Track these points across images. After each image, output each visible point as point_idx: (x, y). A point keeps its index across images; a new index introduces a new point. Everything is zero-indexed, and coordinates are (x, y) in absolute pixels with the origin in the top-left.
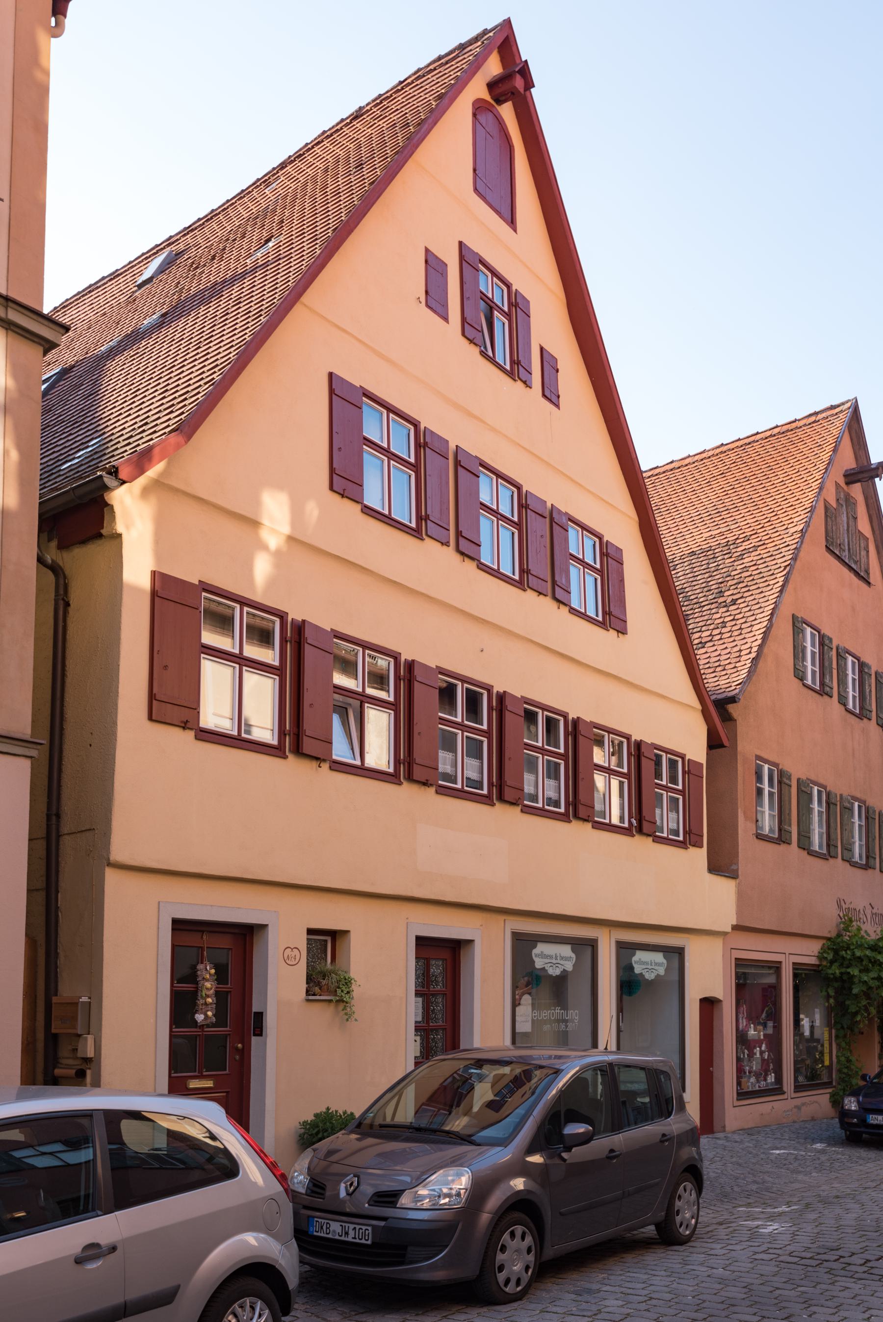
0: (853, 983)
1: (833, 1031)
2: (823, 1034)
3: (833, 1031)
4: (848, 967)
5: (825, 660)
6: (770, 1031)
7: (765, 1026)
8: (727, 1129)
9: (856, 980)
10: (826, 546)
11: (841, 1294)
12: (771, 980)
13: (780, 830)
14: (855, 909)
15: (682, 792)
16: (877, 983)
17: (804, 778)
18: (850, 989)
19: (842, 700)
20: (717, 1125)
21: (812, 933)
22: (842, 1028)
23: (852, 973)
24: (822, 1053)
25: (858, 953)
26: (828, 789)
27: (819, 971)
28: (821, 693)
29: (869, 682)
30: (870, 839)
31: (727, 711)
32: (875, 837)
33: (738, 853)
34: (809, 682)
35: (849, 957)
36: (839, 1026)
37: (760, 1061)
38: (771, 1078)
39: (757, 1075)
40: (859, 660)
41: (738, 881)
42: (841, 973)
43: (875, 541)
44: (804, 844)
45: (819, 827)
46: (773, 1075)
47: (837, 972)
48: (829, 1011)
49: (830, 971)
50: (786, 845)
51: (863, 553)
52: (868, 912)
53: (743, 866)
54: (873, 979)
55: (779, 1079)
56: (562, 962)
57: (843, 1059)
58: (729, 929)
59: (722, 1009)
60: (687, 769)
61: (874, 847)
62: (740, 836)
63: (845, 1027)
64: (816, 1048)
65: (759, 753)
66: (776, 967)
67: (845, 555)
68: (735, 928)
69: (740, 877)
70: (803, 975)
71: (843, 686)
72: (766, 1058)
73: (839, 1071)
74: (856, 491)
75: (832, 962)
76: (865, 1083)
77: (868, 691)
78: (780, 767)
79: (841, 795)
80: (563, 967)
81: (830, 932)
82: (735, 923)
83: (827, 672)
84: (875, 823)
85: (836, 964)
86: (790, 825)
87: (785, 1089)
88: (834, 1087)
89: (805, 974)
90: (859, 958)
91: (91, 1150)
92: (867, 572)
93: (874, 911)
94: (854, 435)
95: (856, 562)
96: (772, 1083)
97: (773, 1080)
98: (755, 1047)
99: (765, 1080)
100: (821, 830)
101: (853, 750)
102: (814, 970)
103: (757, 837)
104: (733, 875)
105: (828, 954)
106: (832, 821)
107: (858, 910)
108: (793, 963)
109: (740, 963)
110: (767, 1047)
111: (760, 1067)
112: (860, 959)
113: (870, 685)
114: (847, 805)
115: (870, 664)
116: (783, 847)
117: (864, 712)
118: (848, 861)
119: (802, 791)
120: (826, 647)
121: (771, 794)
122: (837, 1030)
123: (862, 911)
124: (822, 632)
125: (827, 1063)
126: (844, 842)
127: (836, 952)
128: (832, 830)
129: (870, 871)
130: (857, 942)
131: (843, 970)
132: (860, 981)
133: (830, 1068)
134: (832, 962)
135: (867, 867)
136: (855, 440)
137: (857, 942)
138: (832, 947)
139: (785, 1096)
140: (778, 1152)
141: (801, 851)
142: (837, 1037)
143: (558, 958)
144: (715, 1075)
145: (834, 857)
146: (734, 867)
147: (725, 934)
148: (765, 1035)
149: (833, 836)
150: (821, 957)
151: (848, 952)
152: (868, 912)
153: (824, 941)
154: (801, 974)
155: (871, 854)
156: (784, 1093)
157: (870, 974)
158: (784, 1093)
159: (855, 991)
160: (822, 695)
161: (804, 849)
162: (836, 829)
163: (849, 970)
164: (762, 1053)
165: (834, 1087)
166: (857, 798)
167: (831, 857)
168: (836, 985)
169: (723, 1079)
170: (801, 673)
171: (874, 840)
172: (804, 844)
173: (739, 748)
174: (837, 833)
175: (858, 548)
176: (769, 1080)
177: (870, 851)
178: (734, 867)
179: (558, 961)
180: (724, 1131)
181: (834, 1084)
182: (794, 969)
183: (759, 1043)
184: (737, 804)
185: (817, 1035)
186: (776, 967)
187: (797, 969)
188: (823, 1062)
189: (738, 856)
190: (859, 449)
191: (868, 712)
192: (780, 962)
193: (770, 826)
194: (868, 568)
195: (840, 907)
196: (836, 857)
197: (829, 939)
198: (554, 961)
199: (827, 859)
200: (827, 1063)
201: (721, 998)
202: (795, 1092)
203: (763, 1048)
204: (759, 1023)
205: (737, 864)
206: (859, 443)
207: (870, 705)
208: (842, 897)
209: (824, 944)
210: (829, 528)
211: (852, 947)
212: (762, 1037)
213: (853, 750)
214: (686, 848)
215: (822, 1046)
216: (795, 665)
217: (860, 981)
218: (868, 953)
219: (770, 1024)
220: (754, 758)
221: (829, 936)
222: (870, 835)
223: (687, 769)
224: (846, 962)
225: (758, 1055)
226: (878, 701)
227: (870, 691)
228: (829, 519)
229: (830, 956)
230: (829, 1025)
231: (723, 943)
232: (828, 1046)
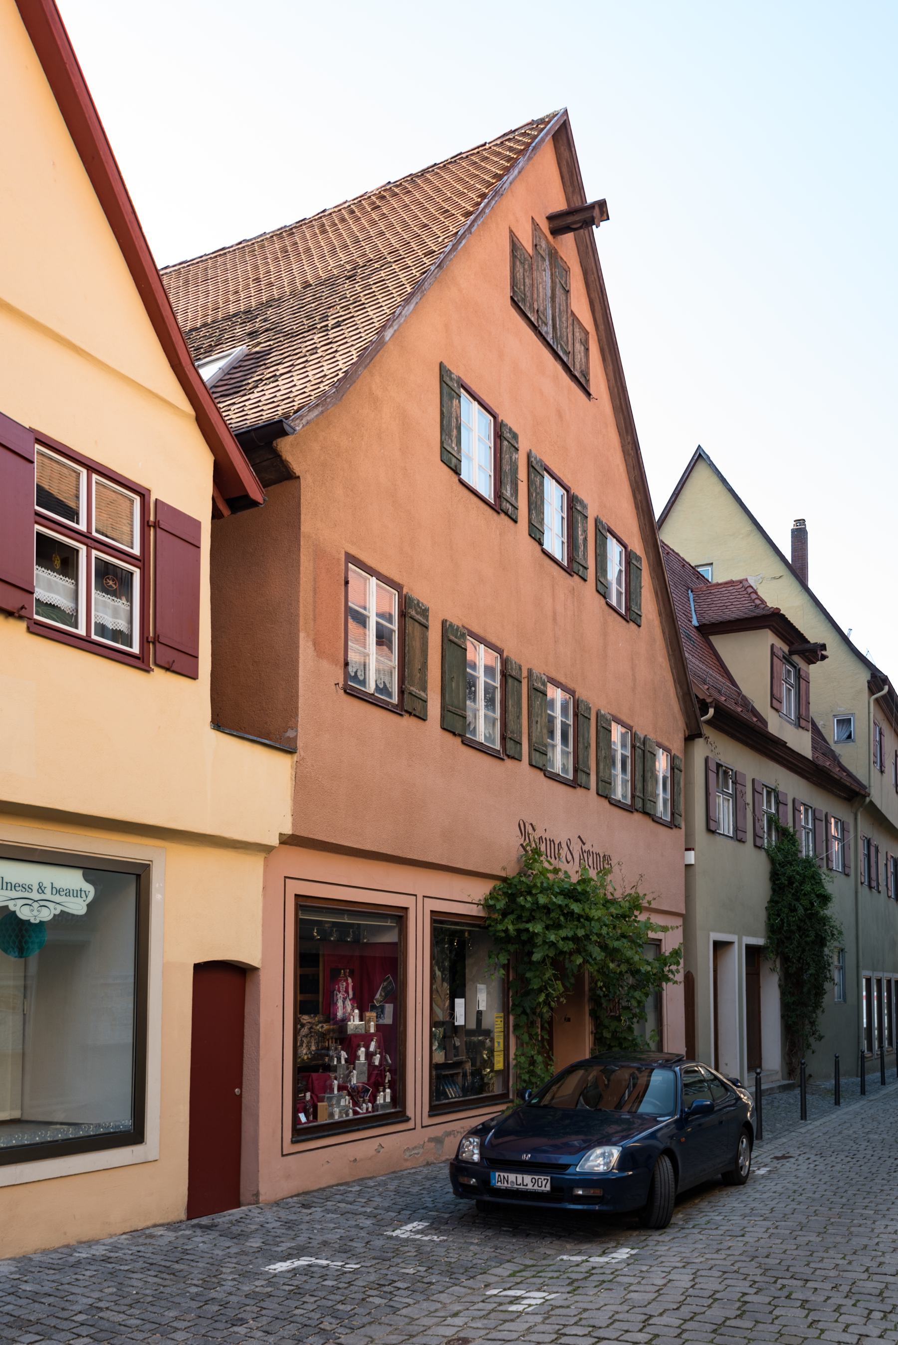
0: (534, 945)
1: (511, 1018)
2: (495, 1021)
3: (511, 1018)
4: (528, 922)
5: (504, 462)
6: (388, 1020)
7: (381, 1012)
8: (261, 1198)
9: (539, 941)
10: (512, 298)
11: (748, 1199)
12: (391, 937)
13: (402, 692)
14: (552, 841)
15: (141, 561)
16: (571, 945)
17: (456, 622)
18: (531, 953)
19: (603, 591)
20: (245, 1193)
21: (470, 868)
22: (524, 1012)
23: (531, 929)
24: (491, 1051)
25: (542, 900)
26: (505, 655)
27: (487, 928)
28: (569, 570)
29: (583, 527)
30: (581, 746)
31: (280, 456)
32: (589, 744)
33: (297, 708)
34: (614, 602)
35: (528, 905)
36: (519, 1010)
37: (365, 1068)
38: (384, 1097)
39: (356, 1095)
40: (568, 491)
41: (296, 757)
42: (519, 931)
43: (599, 341)
44: (604, 793)
45: (486, 706)
46: (388, 1091)
47: (511, 927)
48: (506, 987)
49: (500, 927)
50: (678, 829)
51: (579, 347)
52: (576, 847)
53: (304, 734)
54: (564, 939)
55: (398, 1099)
56: (57, 898)
57: (523, 1059)
58: (275, 841)
59: (258, 984)
60: (152, 518)
61: (587, 757)
62: (301, 679)
63: (528, 1011)
64: (482, 1043)
65: (353, 551)
66: (399, 916)
67: (547, 330)
68: (288, 841)
69: (301, 751)
70: (466, 934)
71: (537, 515)
72: (377, 1063)
73: (518, 1077)
74: (567, 244)
75: (505, 914)
76: (522, 1102)
77: (581, 538)
78: (405, 591)
79: (530, 671)
80: (59, 909)
81: (504, 869)
82: (288, 830)
83: (507, 480)
84: (589, 726)
85: (511, 917)
86: (424, 689)
87: (410, 1112)
88: (512, 1101)
89: (469, 931)
90: (545, 907)
91: (434, 1061)
92: (585, 374)
93: (585, 848)
94: (565, 169)
95: (567, 353)
96: (384, 1106)
97: (388, 1100)
98: (359, 1047)
99: (373, 1099)
100: (490, 714)
101: (555, 613)
102: (479, 926)
103: (345, 692)
104: (290, 750)
105: (498, 900)
106: (510, 703)
107: (557, 843)
108: (432, 911)
109: (303, 903)
110: (378, 1046)
111: (364, 1079)
112: (547, 909)
113: (585, 531)
114: (539, 685)
115: (586, 502)
116: (407, 722)
117: (575, 565)
118: (541, 769)
119: (450, 640)
120: (505, 443)
121: (489, 690)
122: (517, 1016)
123: (564, 845)
124: (500, 419)
125: (499, 1065)
126: (534, 740)
127: (512, 898)
128: (511, 717)
129: (580, 791)
130: (542, 883)
131: (522, 926)
132: (544, 942)
133: (505, 1072)
134: (505, 914)
135: (574, 784)
136: (566, 176)
137: (542, 883)
138: (505, 890)
139: (411, 1124)
140: (281, 1266)
141: (448, 737)
142: (516, 1027)
143: (48, 891)
144: (245, 1100)
145: (513, 758)
146: (290, 734)
147: (265, 849)
148: (378, 1026)
149: (511, 725)
150: (488, 907)
151: (529, 898)
152: (576, 847)
153: (498, 883)
154: (463, 932)
155: (581, 767)
156: (408, 1119)
157: (560, 932)
158: (408, 1119)
159: (536, 957)
160: (498, 513)
161: (454, 734)
162: (519, 717)
163: (530, 926)
164: (369, 1056)
165: (512, 1101)
166: (561, 683)
167: (508, 756)
168: (512, 948)
169: (258, 1108)
170: (454, 460)
171: (587, 747)
172: (604, 793)
173: (306, 527)
174: (520, 724)
175: (570, 336)
176: (380, 1100)
177: (580, 762)
178: (290, 734)
179: (48, 896)
180: (257, 1202)
181: (511, 1097)
182: (433, 921)
183: (366, 1038)
184: (298, 623)
185: (485, 1025)
186: (399, 916)
187: (442, 922)
188: (492, 1066)
189: (297, 715)
190: (573, 192)
191: (581, 568)
192: (406, 909)
193: (563, 765)
194: (588, 367)
195: (523, 832)
196: (517, 758)
197: (504, 880)
198: (35, 895)
199: (503, 759)
200: (499, 1065)
201: (256, 963)
202: (430, 1116)
203: (372, 1047)
204: (374, 1008)
205: (295, 728)
206: (572, 183)
207: (586, 559)
208: (528, 820)
209: (494, 888)
210: (519, 275)
211: (534, 892)
212: (372, 1030)
213: (555, 613)
214: (148, 671)
215: (492, 1040)
216: (442, 443)
217: (544, 942)
218: (559, 900)
219: (389, 1008)
220: (343, 557)
221: (503, 874)
222: (581, 739)
223: (152, 518)
224: (526, 914)
225: (362, 1058)
226: (599, 559)
227: (585, 539)
228: (518, 263)
229: (501, 905)
230: (506, 1010)
231: (266, 866)
232: (501, 1041)
